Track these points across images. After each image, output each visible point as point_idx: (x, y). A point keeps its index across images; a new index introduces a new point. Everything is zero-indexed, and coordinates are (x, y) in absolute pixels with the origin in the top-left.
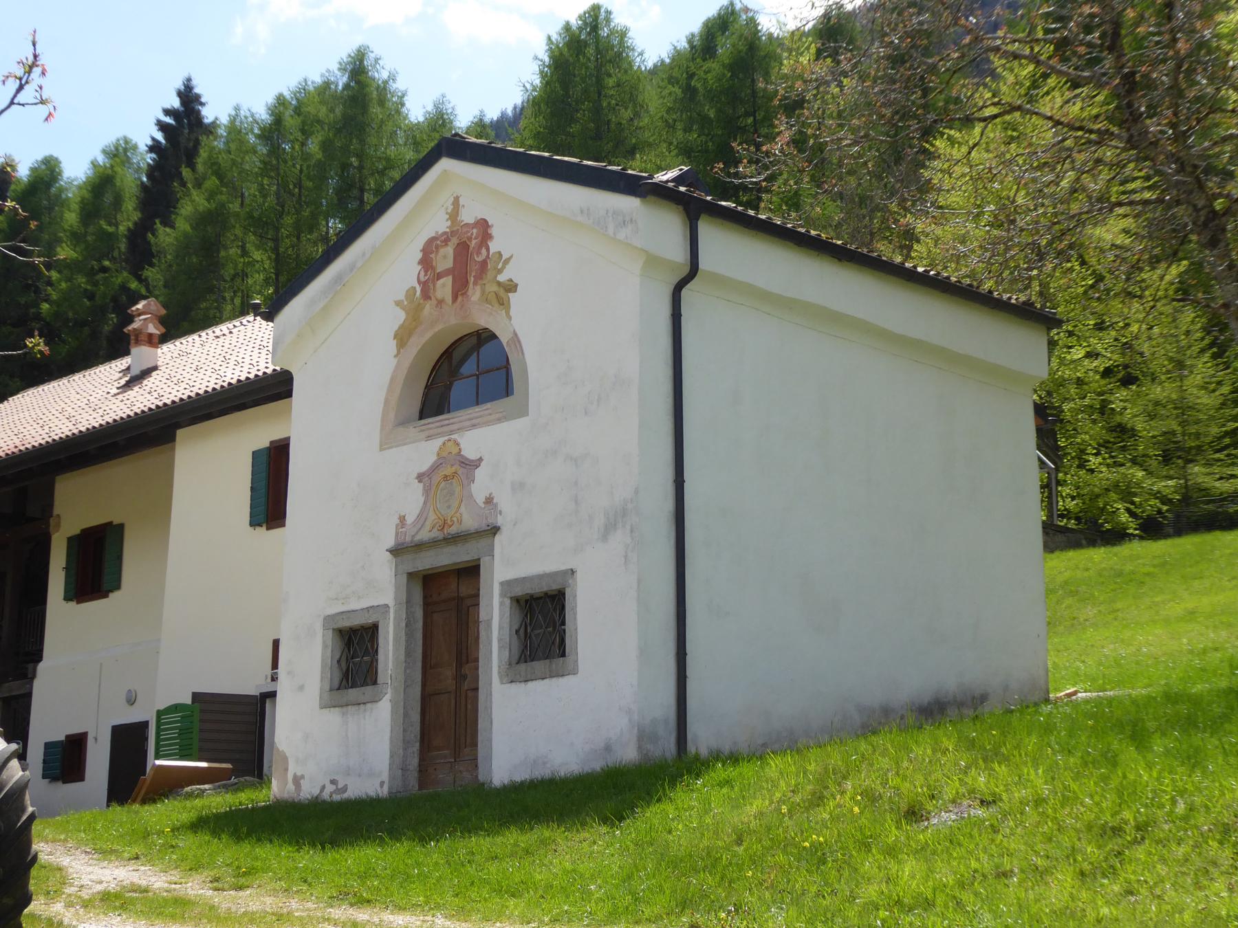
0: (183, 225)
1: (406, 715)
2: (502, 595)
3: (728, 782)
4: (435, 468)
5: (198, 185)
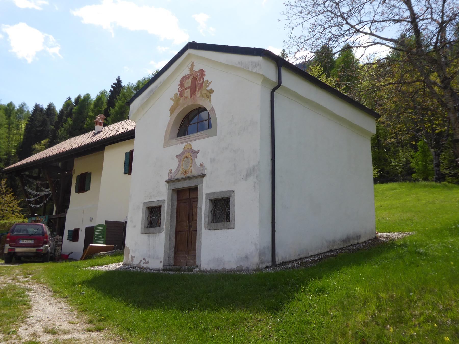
0: (116, 108)
1: (170, 238)
2: (206, 198)
3: (321, 291)
4: (183, 153)
5: (120, 100)
